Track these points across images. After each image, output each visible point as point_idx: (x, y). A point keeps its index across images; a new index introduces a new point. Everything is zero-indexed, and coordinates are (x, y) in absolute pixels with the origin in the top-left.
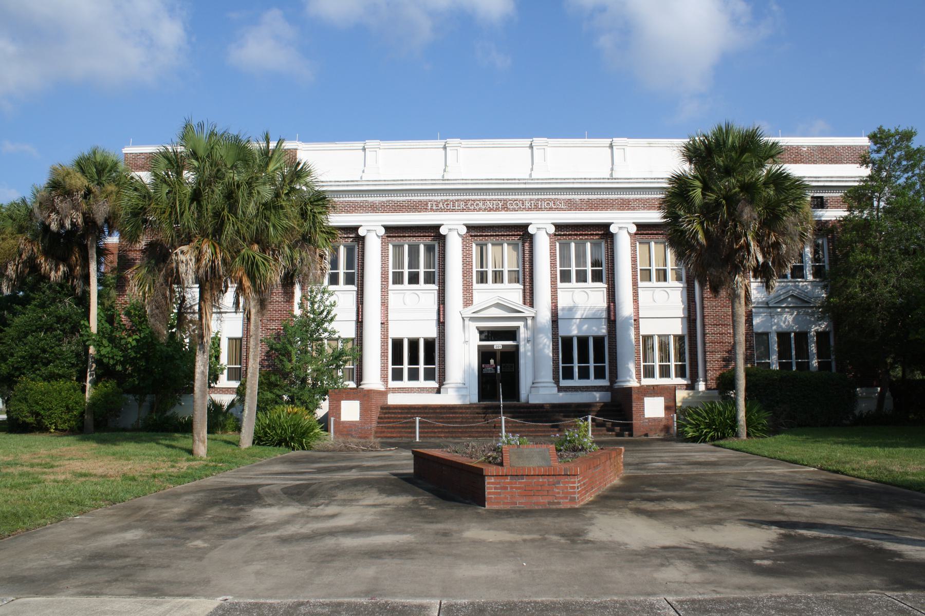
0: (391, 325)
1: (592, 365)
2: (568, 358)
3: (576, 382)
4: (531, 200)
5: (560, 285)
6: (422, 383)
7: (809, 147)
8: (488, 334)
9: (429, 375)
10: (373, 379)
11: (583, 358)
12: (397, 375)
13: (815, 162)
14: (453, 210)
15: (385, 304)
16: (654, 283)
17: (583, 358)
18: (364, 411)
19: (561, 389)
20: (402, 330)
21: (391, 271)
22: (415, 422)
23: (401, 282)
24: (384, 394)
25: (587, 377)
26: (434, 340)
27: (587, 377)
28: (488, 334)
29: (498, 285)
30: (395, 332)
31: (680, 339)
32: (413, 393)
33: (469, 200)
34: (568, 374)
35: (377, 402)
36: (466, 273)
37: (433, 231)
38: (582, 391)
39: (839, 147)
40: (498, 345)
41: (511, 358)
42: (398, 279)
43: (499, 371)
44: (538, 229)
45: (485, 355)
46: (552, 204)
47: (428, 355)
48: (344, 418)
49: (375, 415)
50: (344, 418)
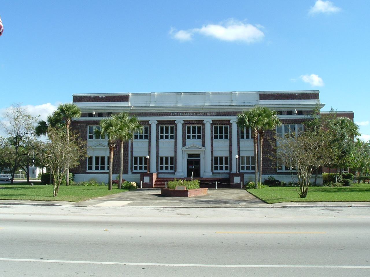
0: (160, 153)
2: (216, 163)
3: (219, 171)
4: (204, 112)
6: (169, 171)
7: (298, 94)
8: (190, 156)
9: (172, 168)
11: (221, 163)
15: (157, 146)
16: (245, 139)
17: (221, 163)
19: (213, 173)
20: (218, 154)
21: (214, 134)
22: (215, 183)
23: (244, 138)
25: (142, 169)
26: (173, 157)
27: (142, 169)
28: (190, 156)
30: (160, 155)
33: (184, 112)
34: (216, 168)
39: (309, 94)
41: (198, 162)
43: (194, 167)
45: (190, 163)
46: (211, 114)
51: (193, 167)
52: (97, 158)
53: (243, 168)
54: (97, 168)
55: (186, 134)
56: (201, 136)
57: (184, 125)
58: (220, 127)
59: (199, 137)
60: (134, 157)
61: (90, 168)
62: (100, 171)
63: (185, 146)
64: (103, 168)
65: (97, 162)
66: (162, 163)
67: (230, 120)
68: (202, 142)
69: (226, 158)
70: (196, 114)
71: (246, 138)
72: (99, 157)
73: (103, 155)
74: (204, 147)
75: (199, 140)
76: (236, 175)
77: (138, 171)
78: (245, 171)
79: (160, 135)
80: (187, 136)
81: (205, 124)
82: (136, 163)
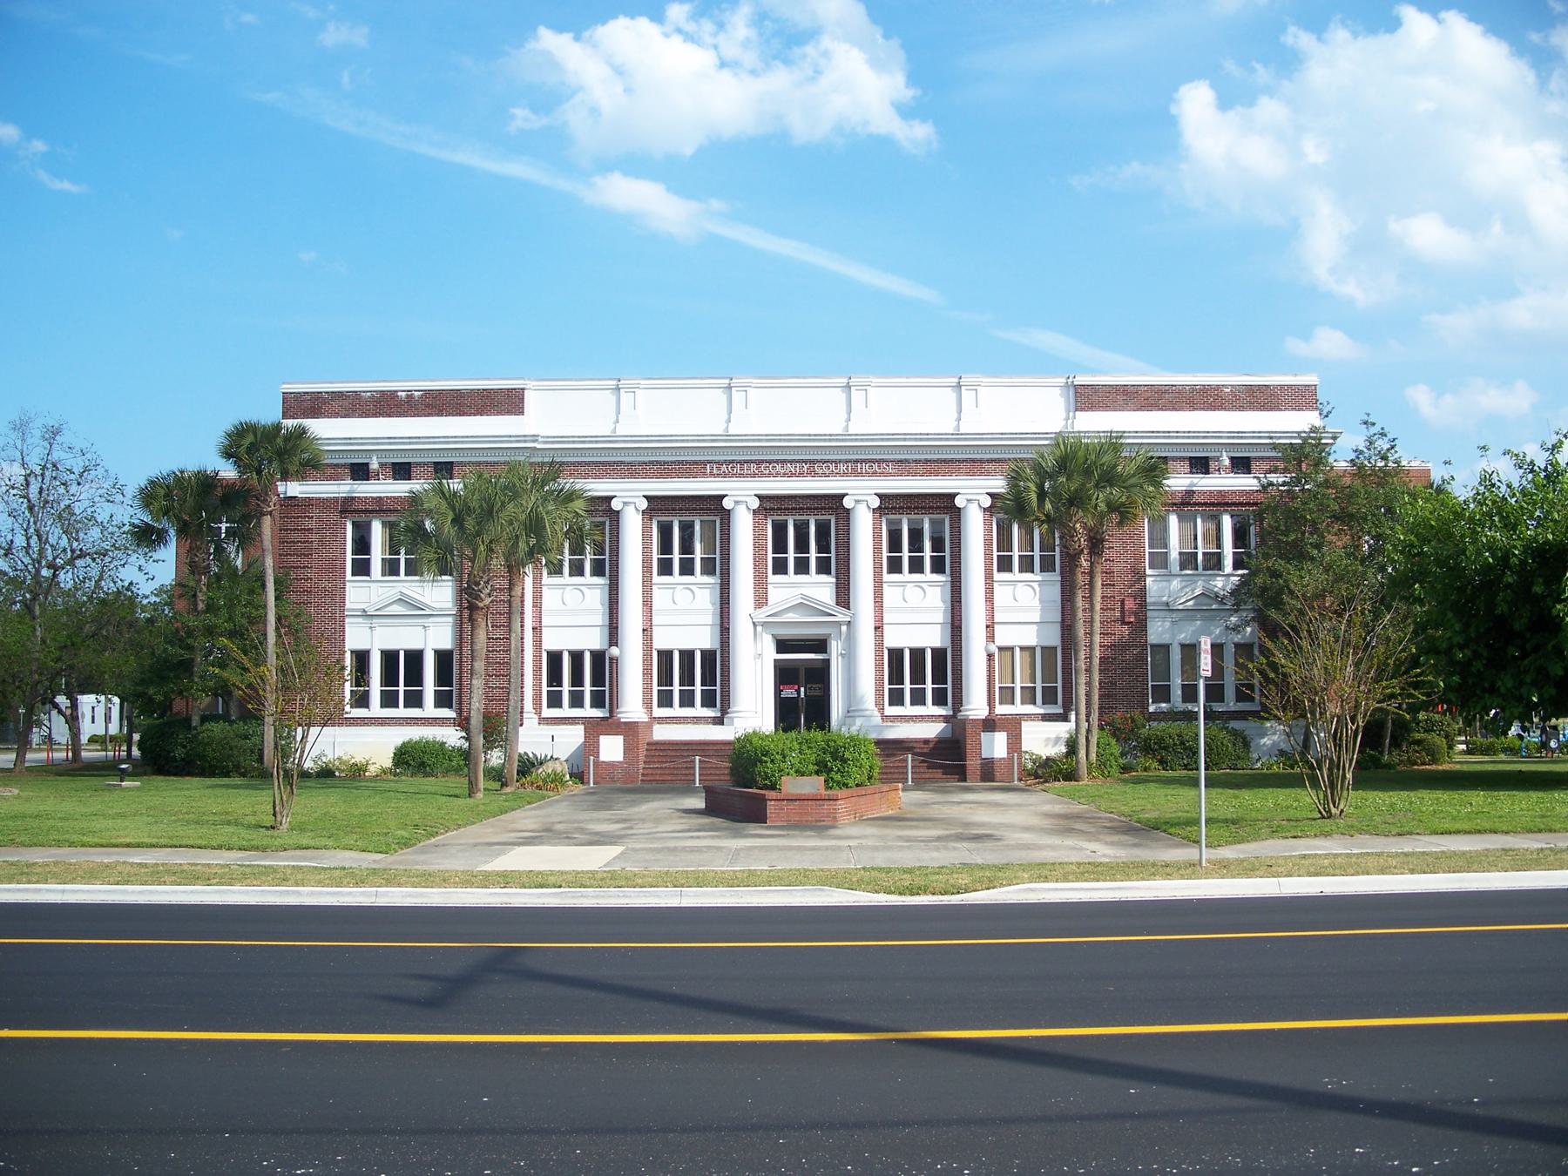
5: (887, 577)
9: (709, 701)
10: (632, 706)
12: (665, 700)
13: (1241, 408)
14: (741, 476)
15: (647, 603)
18: (628, 749)
19: (884, 718)
20: (670, 638)
24: (648, 726)
25: (692, 705)
29: (802, 578)
30: (893, 639)
32: (687, 726)
35: (643, 739)
36: (759, 562)
37: (713, 504)
38: (395, 724)
41: (819, 675)
44: (857, 501)
45: (785, 675)
47: (708, 674)
48: (604, 757)
49: (642, 753)
50: (604, 757)
51: (798, 691)
52: (390, 658)
53: (1008, 696)
55: (770, 555)
58: (819, 525)
59: (824, 567)
60: (659, 652)
61: (362, 700)
62: (401, 711)
64: (415, 700)
65: (389, 677)
67: (952, 496)
70: (811, 464)
71: (819, 572)
73: (414, 645)
75: (824, 578)
76: (990, 724)
77: (566, 711)
78: (1019, 708)
79: (655, 556)
81: (848, 511)
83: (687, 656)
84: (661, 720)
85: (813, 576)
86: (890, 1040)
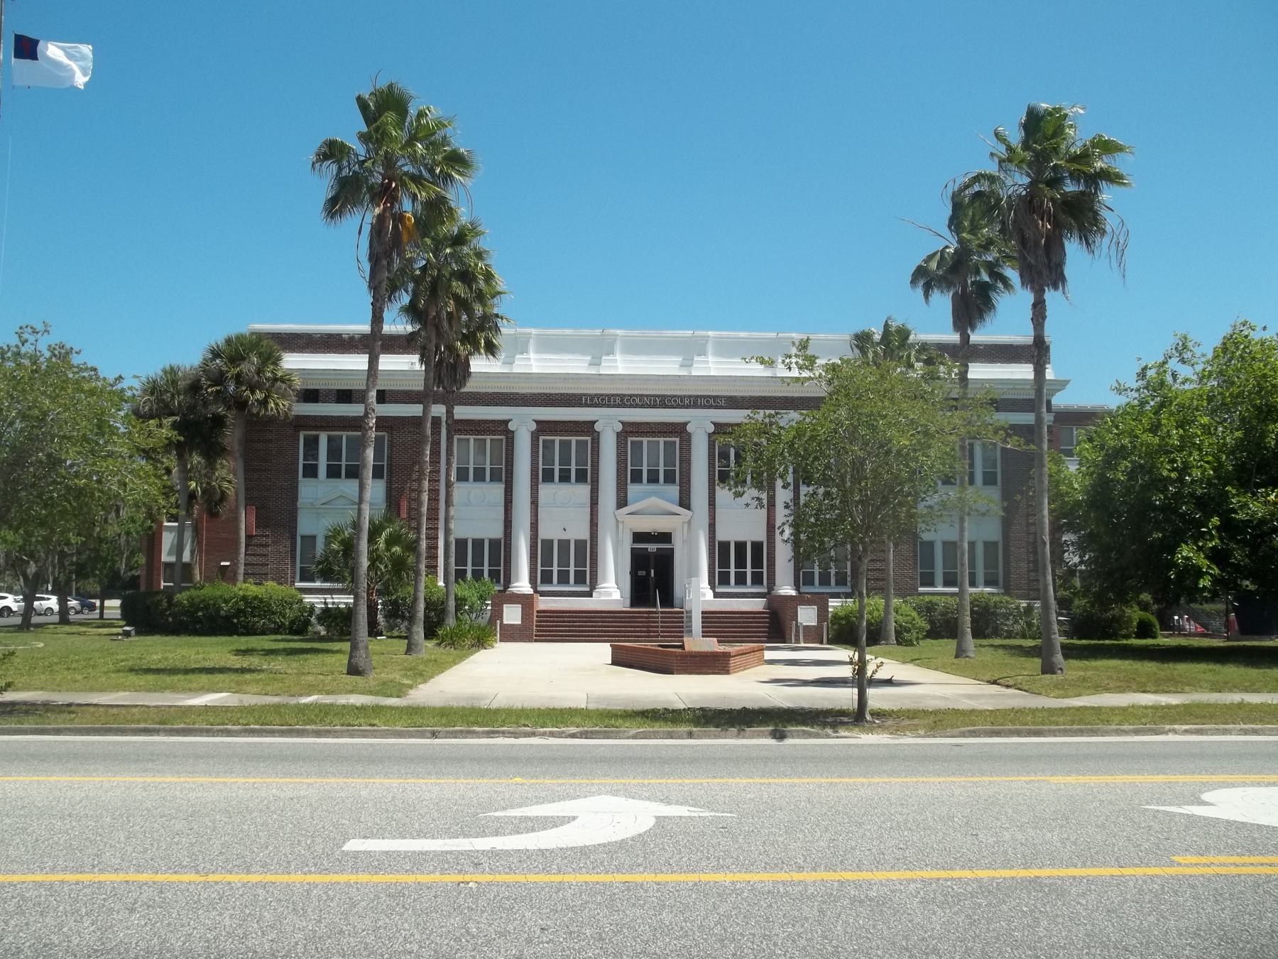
1: (749, 570)
8: (639, 537)
9: (580, 579)
15: (535, 503)
17: (741, 563)
19: (716, 595)
26: (499, 541)
31: (990, 546)
34: (724, 580)
40: (652, 547)
42: (548, 477)
45: (639, 561)
46: (711, 401)
51: (649, 574)
54: (563, 578)
56: (679, 477)
57: (621, 437)
63: (626, 505)
66: (724, 562)
67: (506, 422)
68: (592, 492)
69: (757, 546)
72: (745, 543)
74: (688, 507)
76: (801, 599)
80: (629, 475)
82: (461, 559)
83: (478, 544)
84: (543, 594)
85: (661, 487)
86: (420, 834)
